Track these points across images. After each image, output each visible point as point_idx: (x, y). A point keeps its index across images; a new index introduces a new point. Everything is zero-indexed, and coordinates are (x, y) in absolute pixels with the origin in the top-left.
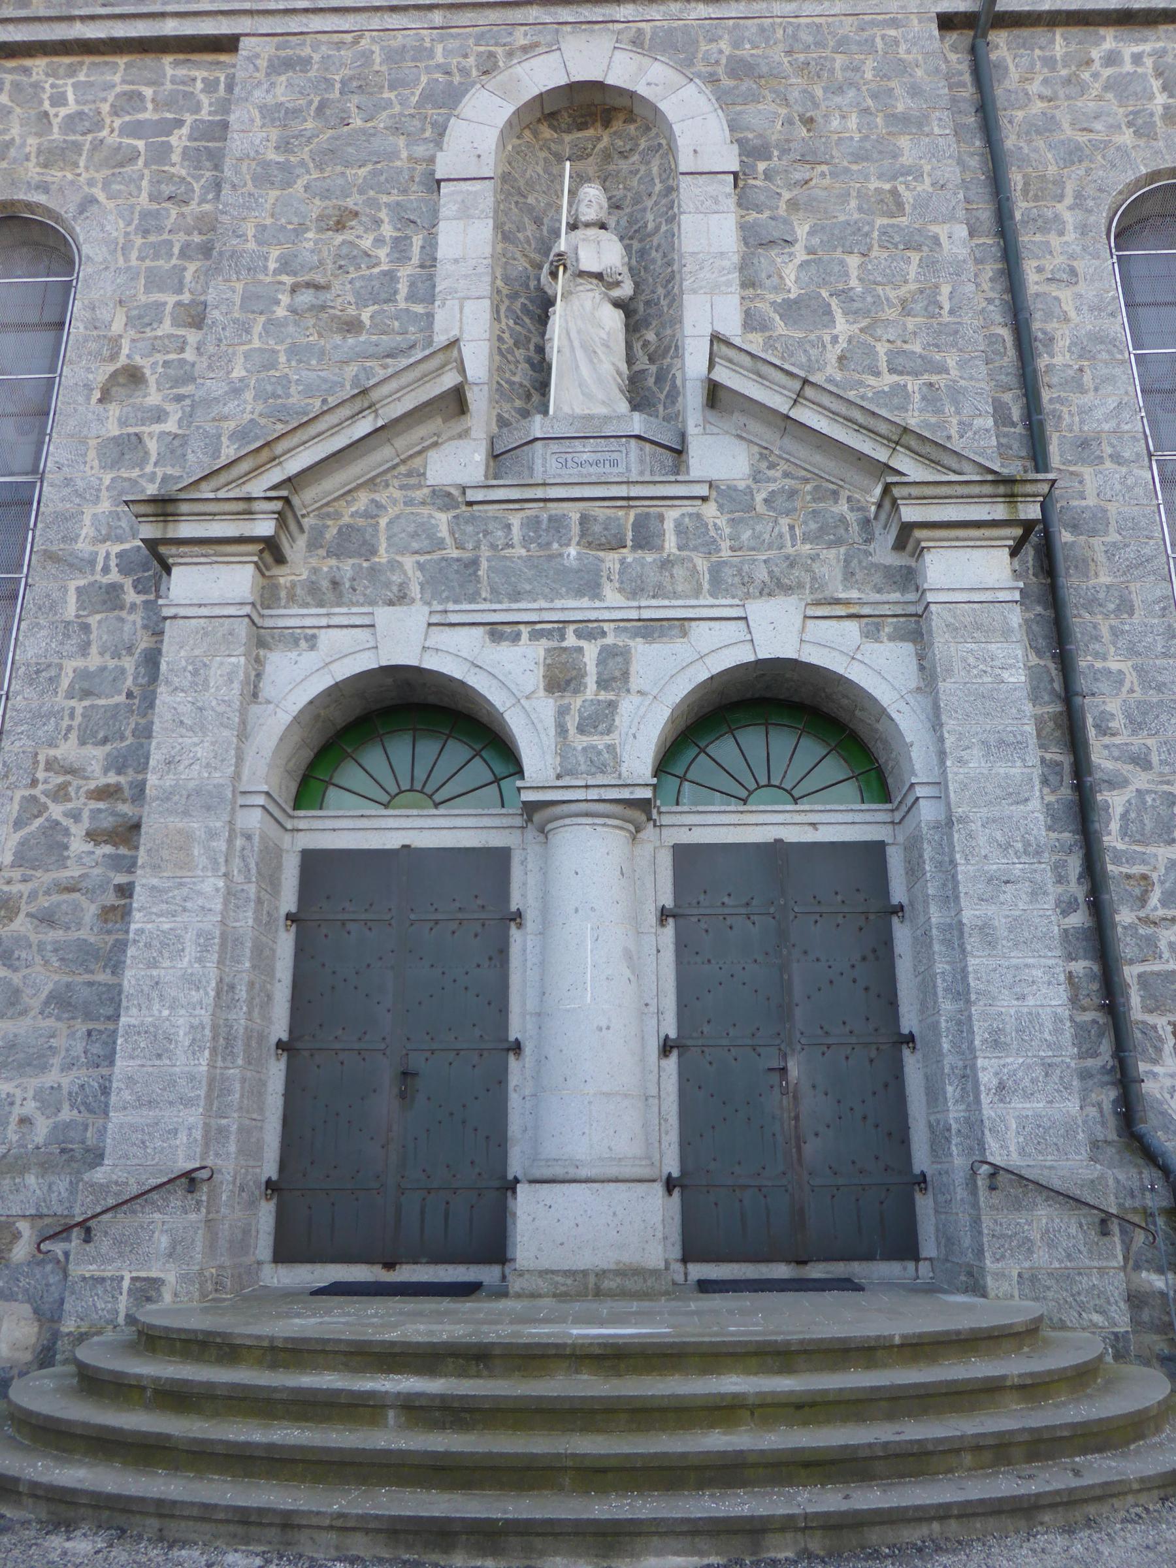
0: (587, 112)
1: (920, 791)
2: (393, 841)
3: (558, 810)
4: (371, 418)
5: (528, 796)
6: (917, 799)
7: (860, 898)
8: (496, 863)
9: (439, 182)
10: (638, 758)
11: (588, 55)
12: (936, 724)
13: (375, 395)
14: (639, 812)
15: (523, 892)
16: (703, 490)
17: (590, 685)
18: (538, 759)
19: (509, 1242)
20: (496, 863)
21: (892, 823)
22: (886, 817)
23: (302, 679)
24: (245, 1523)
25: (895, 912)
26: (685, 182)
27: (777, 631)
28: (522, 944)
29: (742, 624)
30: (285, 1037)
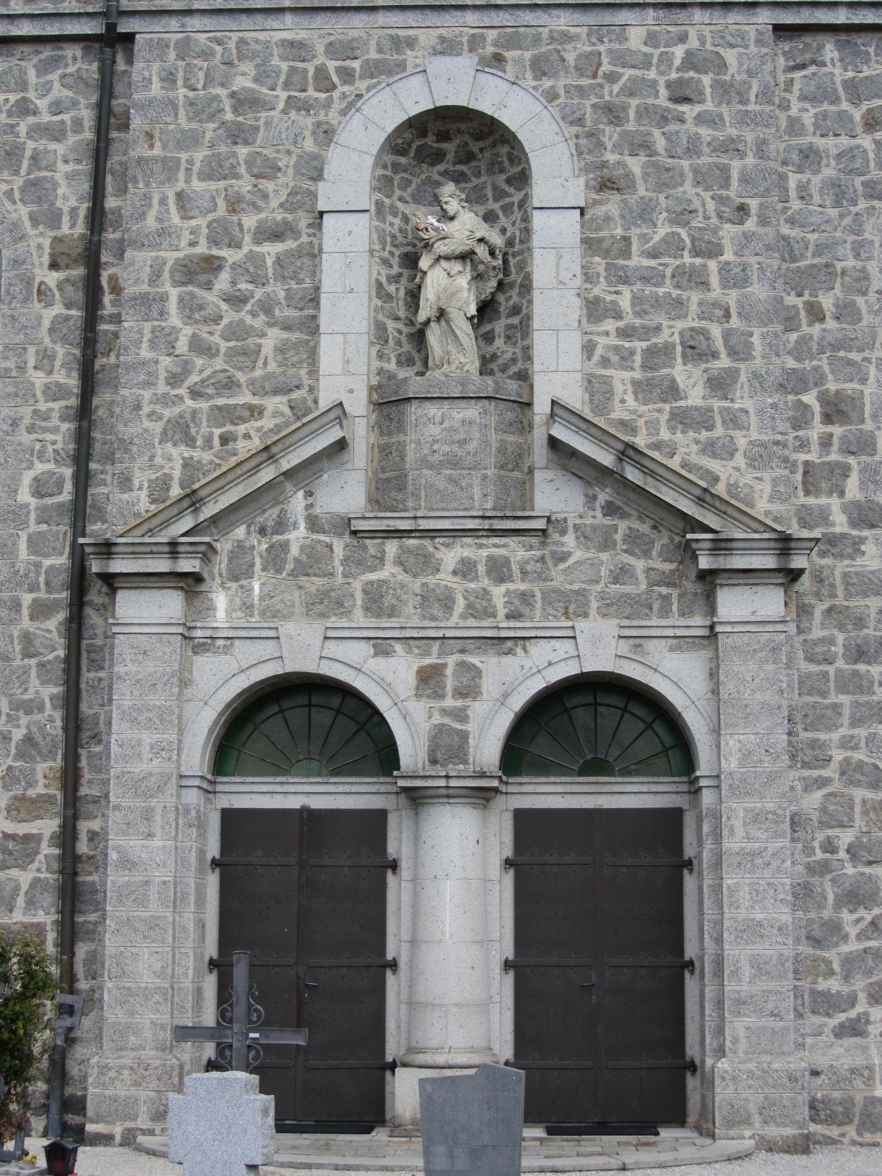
0: (454, 145)
1: (702, 783)
2: (294, 803)
3: (423, 793)
4: (272, 467)
5: (401, 783)
6: (701, 788)
7: (659, 852)
8: (376, 821)
9: (321, 214)
10: (487, 746)
11: (456, 83)
12: (716, 730)
13: (274, 450)
14: (482, 796)
15: (398, 843)
16: (540, 524)
17: (449, 694)
18: (411, 750)
19: (388, 1096)
20: (376, 821)
21: (689, 792)
22: (685, 788)
23: (223, 679)
24: (719, 1002)
25: (686, 866)
26: (536, 213)
27: (597, 647)
28: (398, 891)
29: (572, 641)
30: (215, 955)
